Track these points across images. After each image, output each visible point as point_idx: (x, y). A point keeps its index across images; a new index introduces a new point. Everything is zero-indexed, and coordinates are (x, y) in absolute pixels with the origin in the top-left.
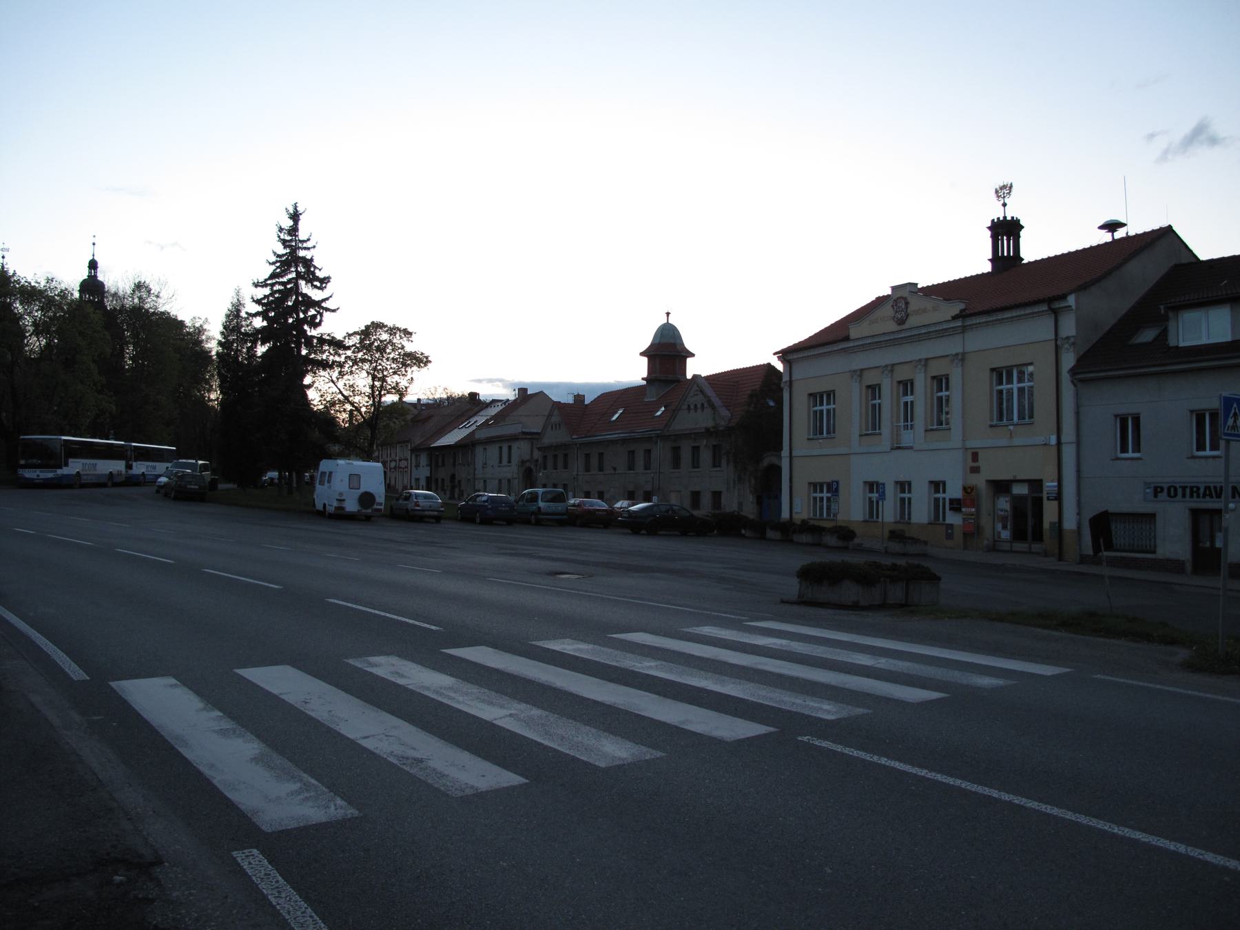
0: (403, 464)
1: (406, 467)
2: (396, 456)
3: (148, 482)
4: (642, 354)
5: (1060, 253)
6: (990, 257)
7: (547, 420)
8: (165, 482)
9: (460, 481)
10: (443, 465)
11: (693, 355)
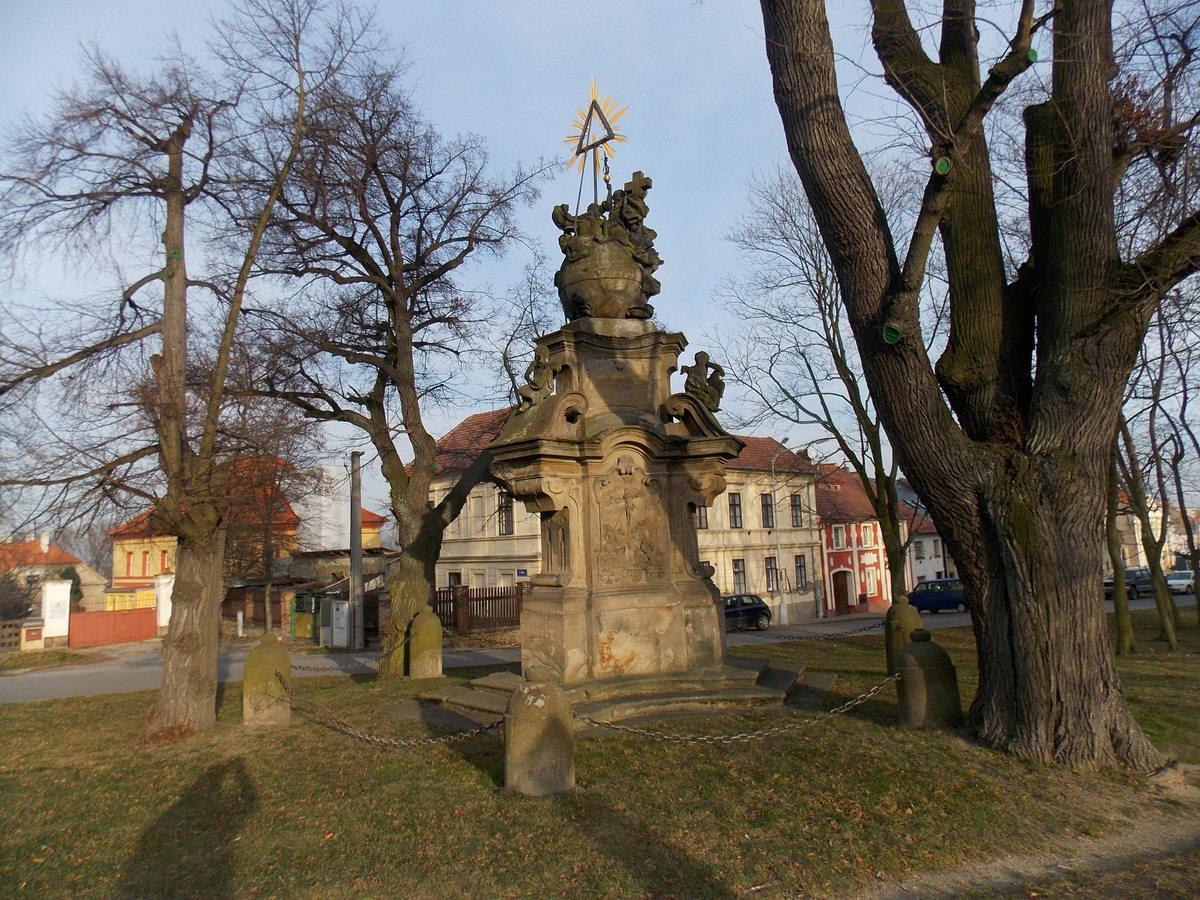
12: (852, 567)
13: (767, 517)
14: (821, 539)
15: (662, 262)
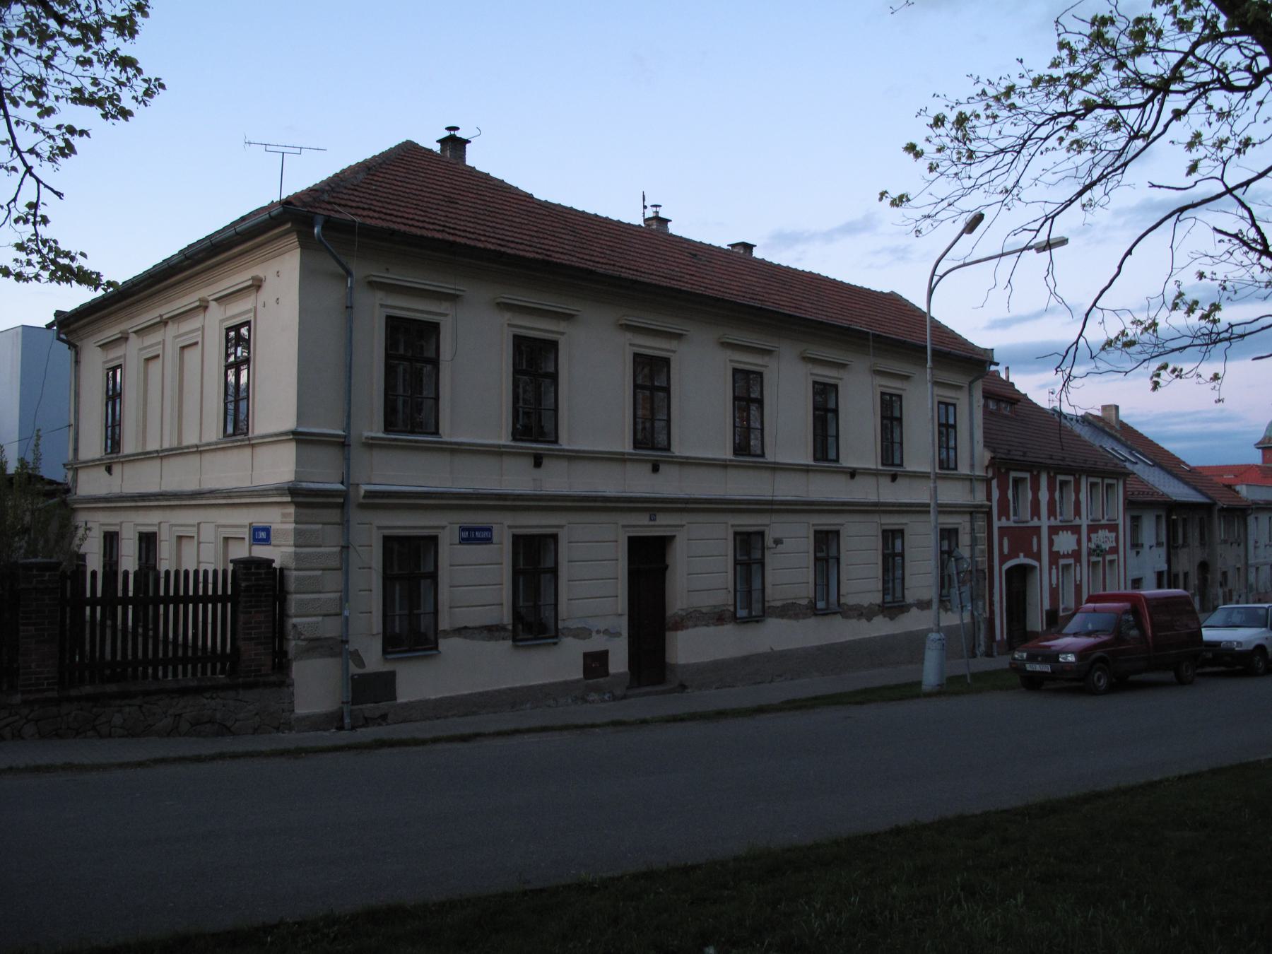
0: (1104, 538)
1: (1114, 550)
2: (1078, 512)
3: (964, 513)
4: (437, 141)
5: (604, 216)
6: (475, 158)
7: (751, 587)
8: (1175, 84)
9: (1225, 574)
10: (1185, 544)
11: (670, 221)
12: (1038, 557)
13: (113, 427)
14: (989, 498)
15: (454, 144)
